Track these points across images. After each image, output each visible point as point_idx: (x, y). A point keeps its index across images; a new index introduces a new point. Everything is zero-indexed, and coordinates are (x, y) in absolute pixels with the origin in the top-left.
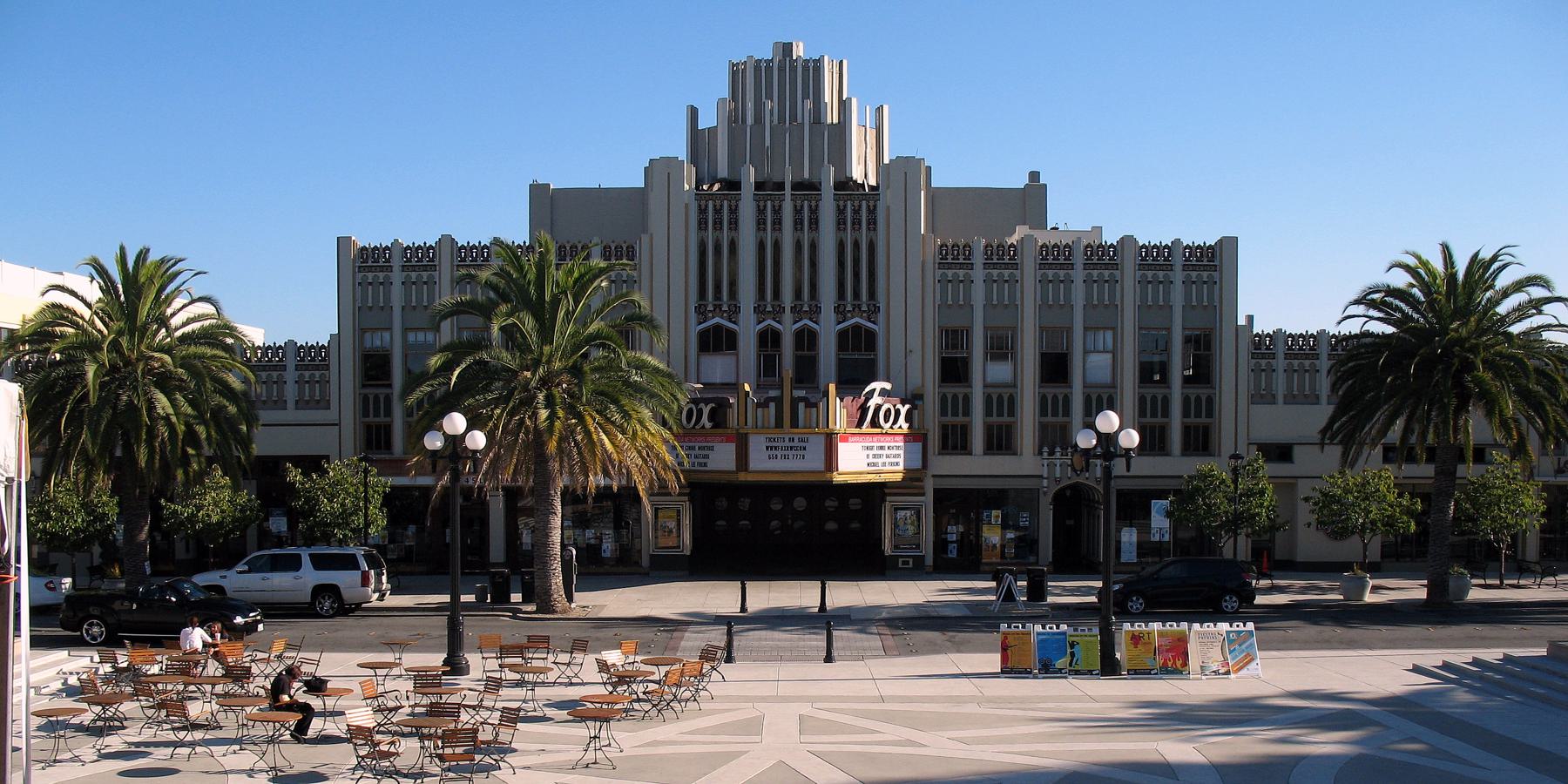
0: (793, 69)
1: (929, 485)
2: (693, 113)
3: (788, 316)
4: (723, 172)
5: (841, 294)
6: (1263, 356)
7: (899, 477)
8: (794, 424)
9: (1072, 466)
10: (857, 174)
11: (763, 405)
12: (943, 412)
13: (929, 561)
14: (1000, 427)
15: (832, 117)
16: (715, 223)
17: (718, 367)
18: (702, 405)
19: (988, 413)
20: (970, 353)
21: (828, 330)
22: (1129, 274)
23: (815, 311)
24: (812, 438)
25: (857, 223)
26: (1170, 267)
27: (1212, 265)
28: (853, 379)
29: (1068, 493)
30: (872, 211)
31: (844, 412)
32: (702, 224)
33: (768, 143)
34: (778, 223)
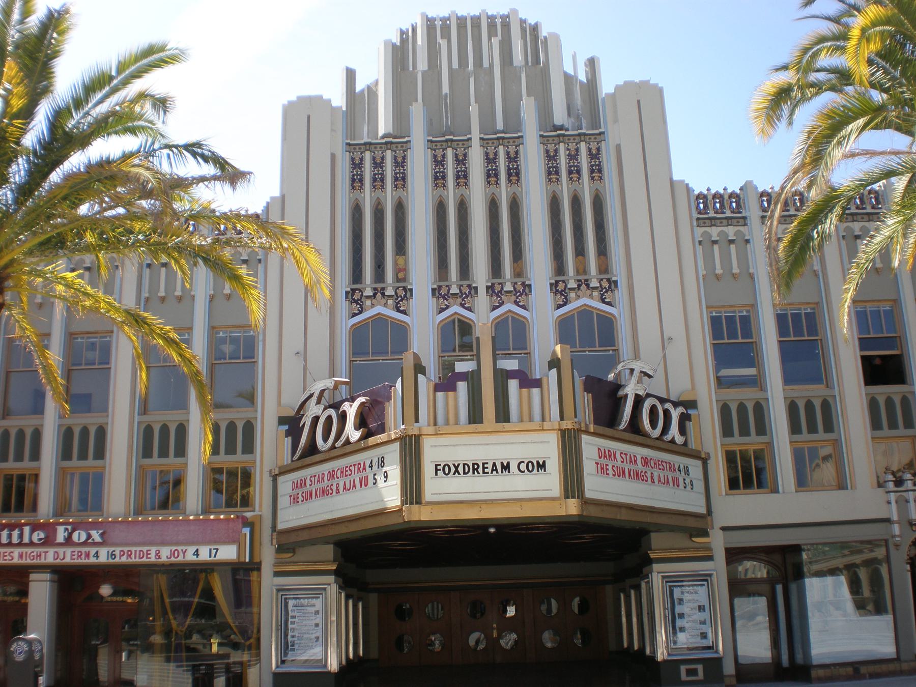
1: (718, 542)
2: (351, 75)
3: (482, 300)
5: (560, 268)
8: (503, 415)
11: (447, 384)
12: (727, 431)
25: (574, 172)
30: (594, 155)
32: (356, 182)
33: (446, 89)
34: (462, 177)
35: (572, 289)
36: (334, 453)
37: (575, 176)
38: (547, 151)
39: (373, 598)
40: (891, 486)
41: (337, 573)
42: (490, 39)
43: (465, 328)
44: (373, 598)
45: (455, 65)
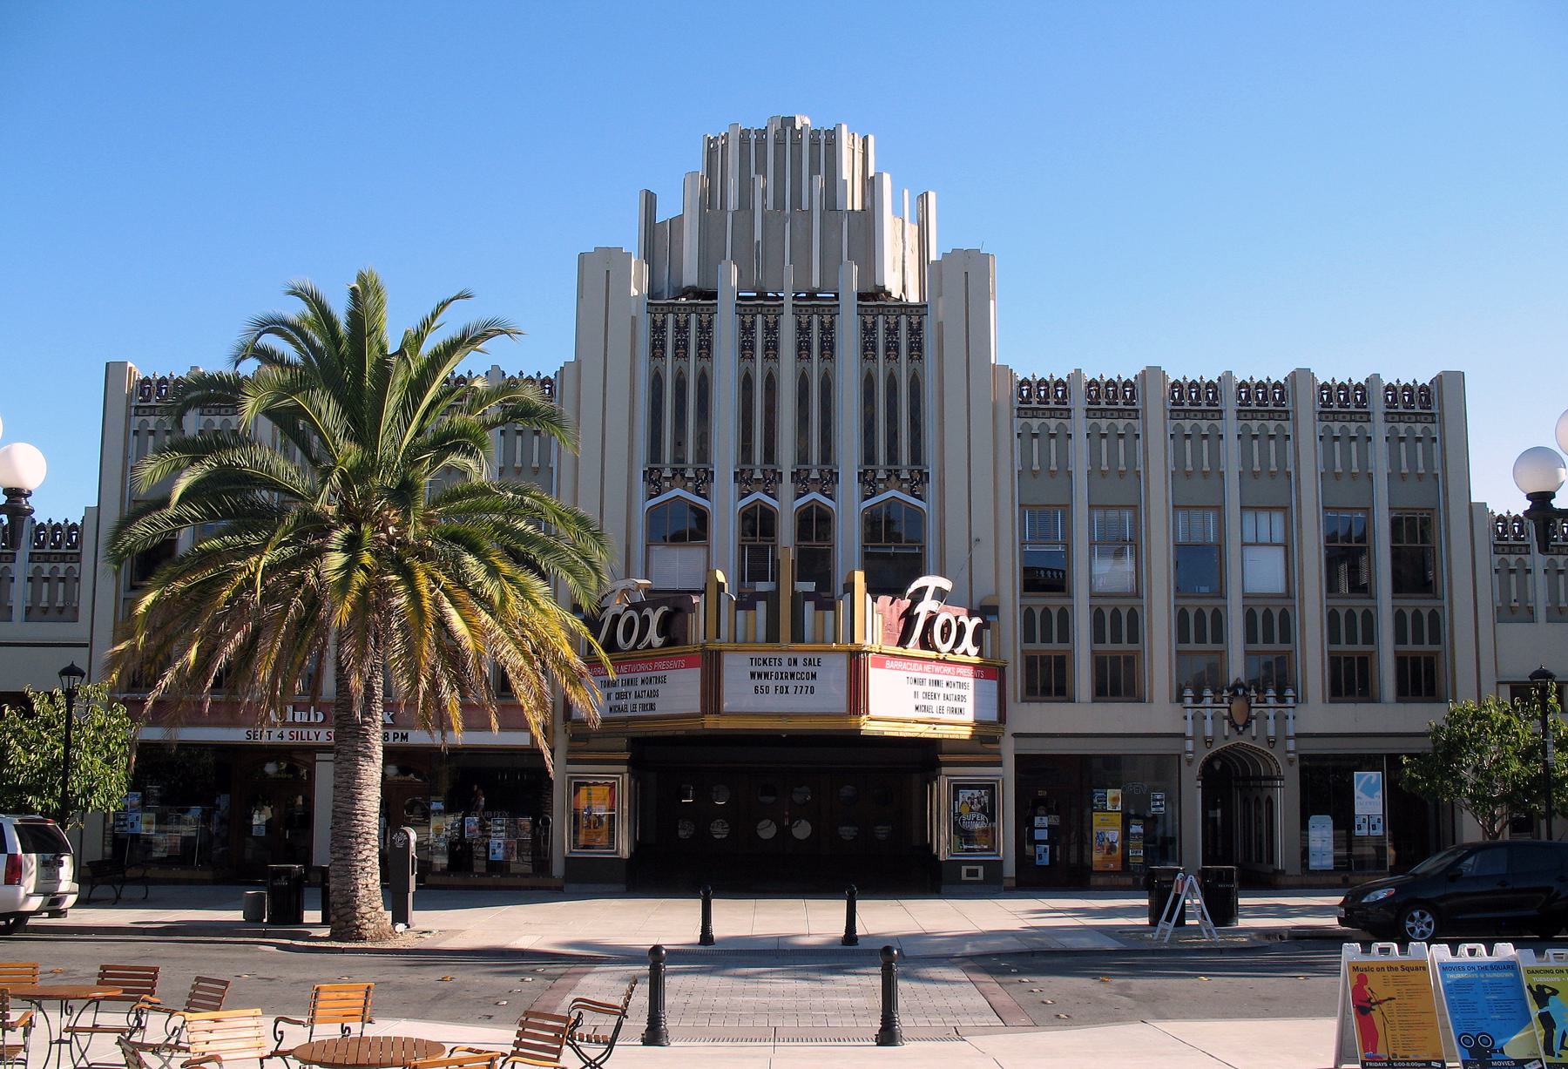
0: (797, 143)
1: (1009, 750)
2: (650, 200)
3: (787, 487)
4: (690, 278)
5: (869, 457)
6: (1511, 549)
7: (965, 733)
8: (798, 636)
9: (1230, 718)
10: (892, 283)
11: (746, 602)
12: (1029, 636)
13: (1010, 870)
14: (1115, 660)
15: (854, 200)
16: (677, 347)
17: (677, 567)
18: (648, 611)
19: (1098, 636)
20: (1068, 546)
21: (849, 510)
22: (1307, 426)
23: (829, 480)
24: (825, 658)
25: (892, 348)
26: (1367, 417)
28: (891, 577)
29: (1217, 765)
30: (916, 331)
31: (878, 619)
32: (657, 348)
33: (758, 236)
34: (772, 348)
35: (881, 480)
36: (634, 654)
37: (892, 353)
40: (1189, 701)
41: (628, 762)
42: (811, 178)
45: (770, 207)
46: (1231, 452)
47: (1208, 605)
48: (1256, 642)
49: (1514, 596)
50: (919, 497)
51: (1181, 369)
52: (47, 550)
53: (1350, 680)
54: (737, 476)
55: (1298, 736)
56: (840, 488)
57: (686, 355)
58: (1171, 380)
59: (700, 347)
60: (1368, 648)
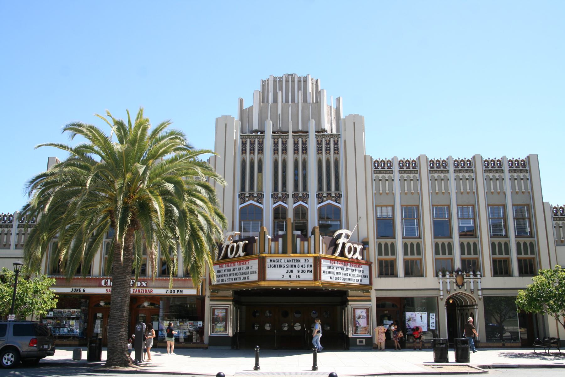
1: (373, 295)
2: (241, 101)
3: (290, 200)
4: (256, 127)
5: (320, 189)
8: (294, 251)
9: (456, 283)
10: (327, 127)
12: (380, 253)
15: (311, 99)
21: (313, 207)
23: (305, 198)
25: (328, 150)
27: (524, 168)
30: (336, 143)
32: (244, 151)
33: (280, 112)
34: (285, 150)
35: (325, 197)
36: (234, 259)
38: (318, 141)
39: (244, 308)
40: (440, 276)
41: (232, 301)
43: (284, 210)
44: (244, 308)
46: (452, 185)
47: (415, 241)
48: (464, 254)
49: (562, 236)
50: (338, 203)
51: (434, 156)
52: (7, 224)
53: (501, 268)
54: (273, 196)
55: (482, 289)
56: (265, 200)
57: (254, 153)
58: (484, 159)
59: (259, 150)
60: (507, 256)
